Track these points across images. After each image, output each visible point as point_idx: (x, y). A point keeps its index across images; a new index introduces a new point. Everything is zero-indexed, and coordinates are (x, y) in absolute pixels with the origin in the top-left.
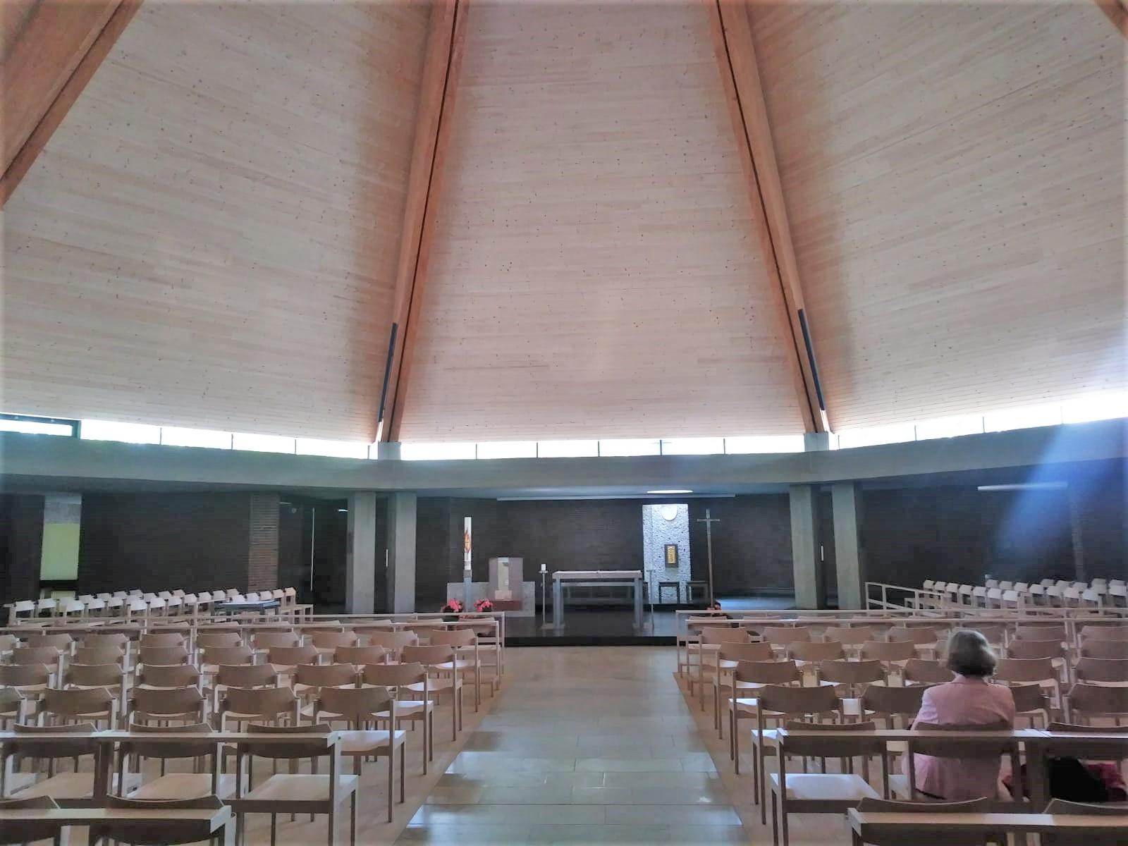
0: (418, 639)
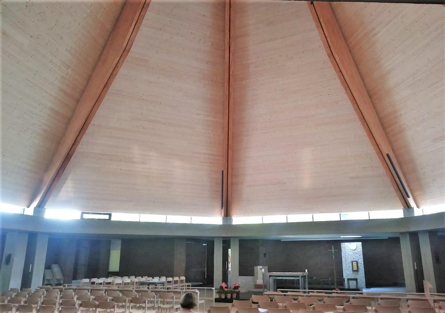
0: (156, 296)
